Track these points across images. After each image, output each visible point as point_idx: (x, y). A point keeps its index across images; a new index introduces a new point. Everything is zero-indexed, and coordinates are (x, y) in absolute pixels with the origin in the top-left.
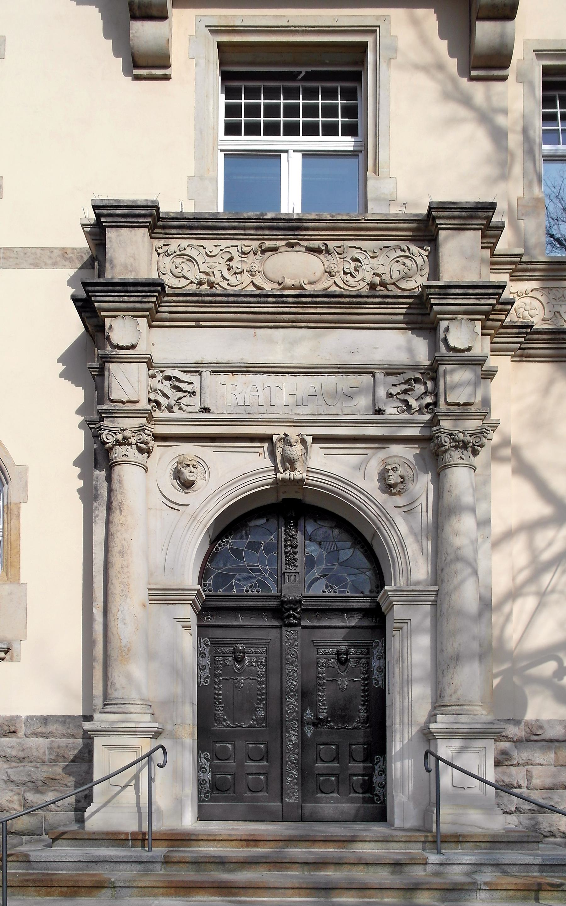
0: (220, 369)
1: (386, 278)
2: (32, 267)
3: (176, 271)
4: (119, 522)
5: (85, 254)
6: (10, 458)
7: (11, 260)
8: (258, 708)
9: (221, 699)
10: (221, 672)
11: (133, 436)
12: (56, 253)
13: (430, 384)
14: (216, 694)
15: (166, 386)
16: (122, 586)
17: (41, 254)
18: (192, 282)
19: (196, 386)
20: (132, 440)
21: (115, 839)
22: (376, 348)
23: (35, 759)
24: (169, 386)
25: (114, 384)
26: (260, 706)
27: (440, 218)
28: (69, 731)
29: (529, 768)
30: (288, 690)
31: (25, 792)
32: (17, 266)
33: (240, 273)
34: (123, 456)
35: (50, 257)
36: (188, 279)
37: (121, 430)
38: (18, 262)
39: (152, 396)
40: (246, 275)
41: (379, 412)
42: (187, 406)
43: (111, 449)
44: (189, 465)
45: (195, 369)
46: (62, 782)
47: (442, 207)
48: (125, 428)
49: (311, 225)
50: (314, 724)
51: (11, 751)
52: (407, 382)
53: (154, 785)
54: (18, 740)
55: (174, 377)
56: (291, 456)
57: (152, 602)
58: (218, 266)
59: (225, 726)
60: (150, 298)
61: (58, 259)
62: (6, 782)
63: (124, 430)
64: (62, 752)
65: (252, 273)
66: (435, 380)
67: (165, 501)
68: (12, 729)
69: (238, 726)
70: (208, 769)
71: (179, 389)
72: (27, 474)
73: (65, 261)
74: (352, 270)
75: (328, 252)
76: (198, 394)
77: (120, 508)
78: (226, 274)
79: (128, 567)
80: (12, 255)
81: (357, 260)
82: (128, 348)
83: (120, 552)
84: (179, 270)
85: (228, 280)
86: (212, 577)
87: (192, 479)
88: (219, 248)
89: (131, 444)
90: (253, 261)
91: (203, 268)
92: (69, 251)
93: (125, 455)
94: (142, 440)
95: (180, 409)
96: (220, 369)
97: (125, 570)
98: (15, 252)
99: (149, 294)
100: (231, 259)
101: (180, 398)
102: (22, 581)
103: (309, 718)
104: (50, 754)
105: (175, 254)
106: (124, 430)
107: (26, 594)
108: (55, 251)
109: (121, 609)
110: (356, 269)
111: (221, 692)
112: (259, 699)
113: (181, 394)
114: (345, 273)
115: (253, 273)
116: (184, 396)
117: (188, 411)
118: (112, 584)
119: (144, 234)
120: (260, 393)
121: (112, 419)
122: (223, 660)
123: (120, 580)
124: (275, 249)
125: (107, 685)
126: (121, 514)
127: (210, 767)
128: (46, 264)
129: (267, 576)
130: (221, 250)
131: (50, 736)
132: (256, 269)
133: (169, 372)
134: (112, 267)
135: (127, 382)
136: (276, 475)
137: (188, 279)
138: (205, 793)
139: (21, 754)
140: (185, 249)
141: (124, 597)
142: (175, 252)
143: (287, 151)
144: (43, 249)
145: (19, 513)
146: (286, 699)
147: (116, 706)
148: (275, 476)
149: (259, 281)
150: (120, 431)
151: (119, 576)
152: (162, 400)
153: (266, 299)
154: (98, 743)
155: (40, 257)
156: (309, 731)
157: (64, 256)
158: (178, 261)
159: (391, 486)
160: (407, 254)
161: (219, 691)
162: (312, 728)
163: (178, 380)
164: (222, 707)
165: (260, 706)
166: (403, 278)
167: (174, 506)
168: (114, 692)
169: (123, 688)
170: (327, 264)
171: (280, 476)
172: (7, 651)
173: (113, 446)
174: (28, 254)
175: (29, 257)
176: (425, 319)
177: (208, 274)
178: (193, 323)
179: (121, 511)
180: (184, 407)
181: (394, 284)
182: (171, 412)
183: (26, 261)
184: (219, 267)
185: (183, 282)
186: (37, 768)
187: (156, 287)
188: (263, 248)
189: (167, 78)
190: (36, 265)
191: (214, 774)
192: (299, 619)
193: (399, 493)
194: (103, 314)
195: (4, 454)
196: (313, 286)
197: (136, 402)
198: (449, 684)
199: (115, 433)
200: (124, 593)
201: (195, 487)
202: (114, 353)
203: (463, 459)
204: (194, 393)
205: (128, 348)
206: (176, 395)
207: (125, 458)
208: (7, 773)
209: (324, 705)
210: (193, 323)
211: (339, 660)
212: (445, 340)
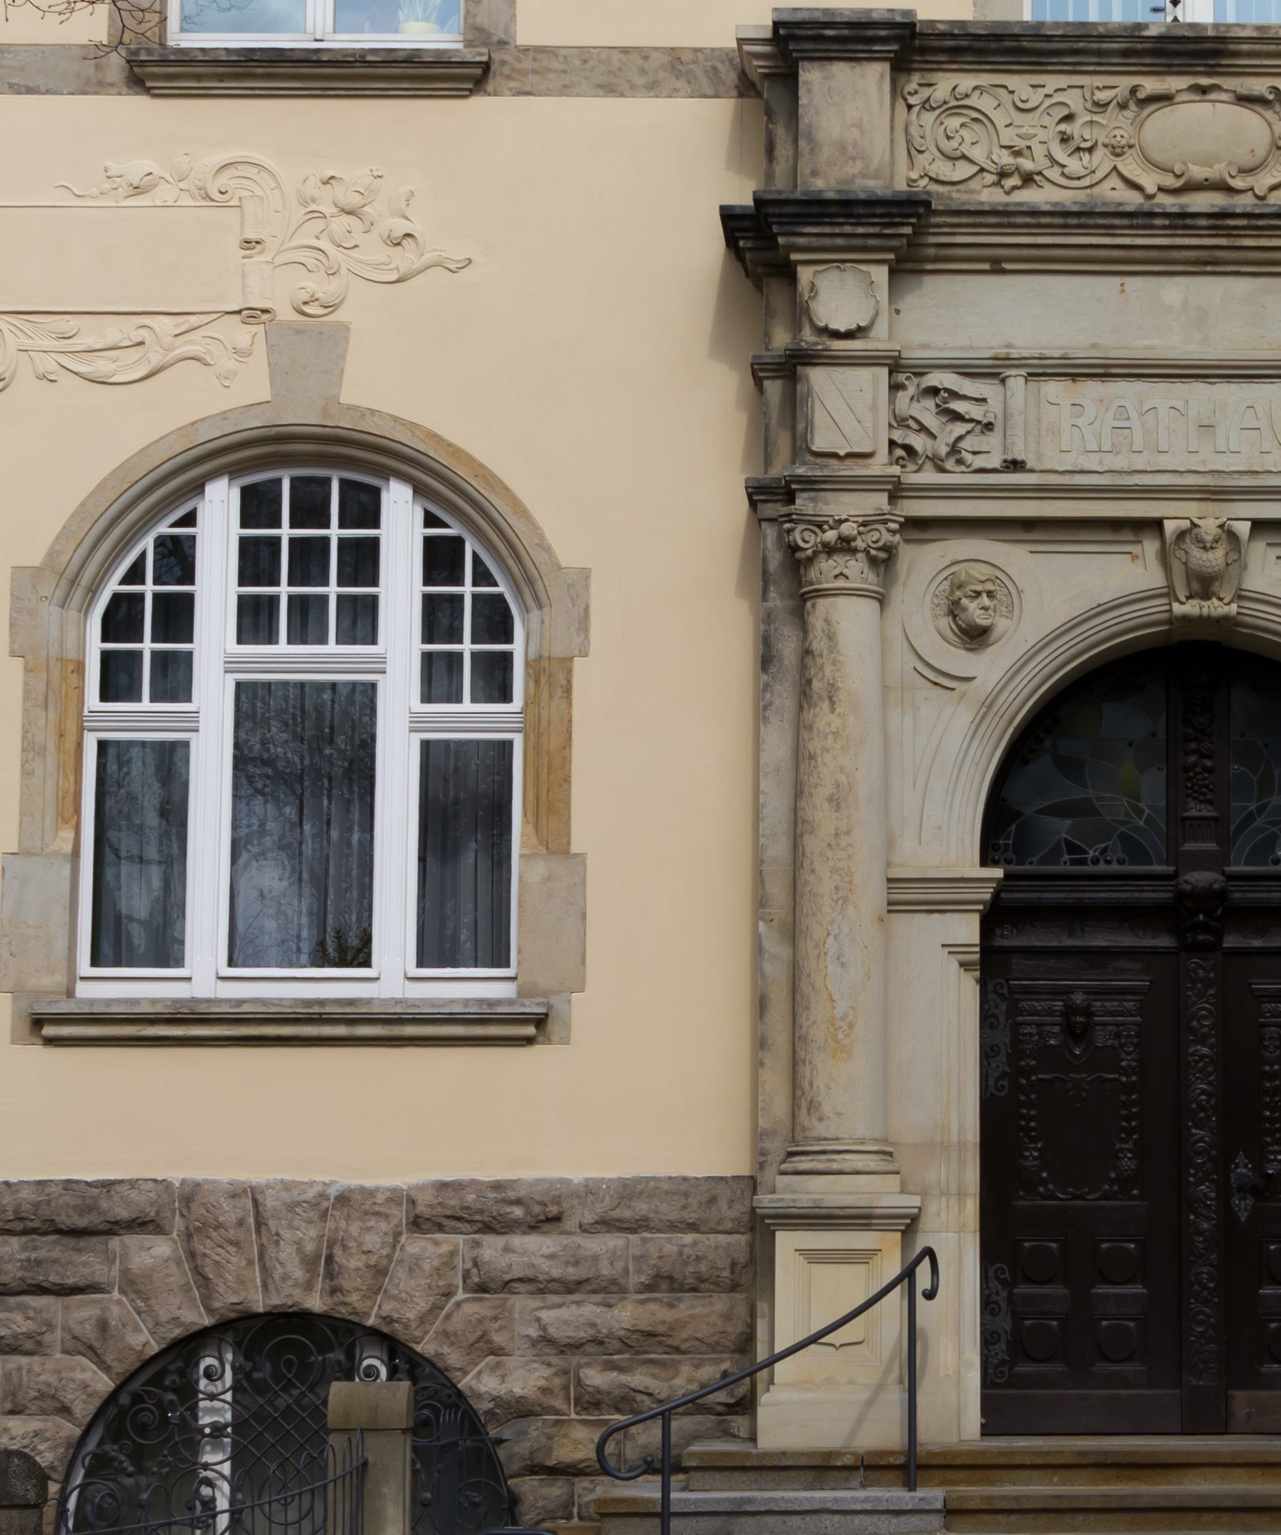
2: (601, 92)
3: (948, 146)
4: (828, 730)
5: (723, 62)
6: (548, 550)
7: (552, 76)
8: (1122, 1150)
9: (1033, 1129)
10: (1033, 1063)
11: (860, 533)
12: (658, 59)
14: (1022, 1117)
15: (926, 412)
16: (836, 877)
17: (621, 62)
18: (982, 170)
20: (859, 544)
23: (604, 1284)
24: (934, 410)
25: (819, 417)
26: (1124, 1146)
30: (1194, 1106)
31: (580, 1366)
32: (565, 90)
34: (836, 577)
35: (643, 71)
36: (974, 163)
37: (836, 521)
38: (567, 82)
39: (898, 436)
40: (1100, 153)
42: (974, 453)
43: (810, 560)
46: (670, 1341)
48: (844, 517)
49: (1245, 47)
51: (550, 1266)
53: (877, 1345)
54: (566, 1240)
55: (946, 390)
56: (1204, 570)
57: (894, 907)
58: (1041, 134)
59: (1044, 1198)
60: (904, 232)
61: (661, 74)
63: (841, 522)
65: (1117, 151)
67: (921, 668)
68: (553, 1210)
69: (1075, 1198)
70: (1004, 1304)
71: (957, 417)
72: (587, 587)
73: (677, 78)
76: (998, 427)
77: (830, 698)
78: (1060, 154)
79: (848, 833)
80: (555, 65)
82: (849, 335)
84: (954, 144)
85: (1064, 166)
86: (1013, 827)
88: (1041, 92)
90: (1118, 125)
91: (1008, 137)
93: (841, 574)
94: (880, 544)
95: (960, 462)
97: (843, 841)
98: (561, 59)
99: (897, 220)
100: (1069, 118)
101: (960, 438)
102: (575, 849)
103: (1244, 1175)
104: (639, 1272)
105: (945, 107)
106: (841, 522)
107: (585, 878)
108: (654, 55)
111: (1033, 1112)
112: (1123, 1130)
113: (960, 428)
115: (1118, 150)
116: (968, 432)
117: (976, 465)
118: (813, 871)
119: (882, 75)
120: (1135, 423)
121: (812, 494)
122: (1040, 1034)
123: (831, 863)
125: (799, 1107)
126: (833, 710)
128: (633, 87)
129: (1141, 823)
130: (1047, 96)
131: (641, 1227)
132: (1124, 142)
133: (935, 379)
134: (812, 150)
135: (847, 408)
136: (1170, 604)
137: (974, 163)
138: (997, 1366)
139: (572, 1273)
140: (967, 96)
141: (840, 902)
142: (945, 102)
144: (625, 51)
145: (569, 682)
146: (1189, 1128)
147: (823, 1157)
148: (1167, 608)
149: (1130, 167)
150: (831, 522)
151: (829, 854)
152: (918, 442)
153: (1148, 221)
154: (787, 1243)
155: (619, 69)
156: (1243, 1206)
157: (673, 67)
161: (1030, 1109)
163: (954, 395)
164: (1036, 1149)
165: (1124, 1146)
167: (944, 681)
168: (814, 1121)
169: (839, 1114)
171: (1178, 609)
173: (815, 553)
174: (591, 63)
175: (592, 69)
177: (1018, 154)
178: (986, 266)
179: (832, 703)
180: (968, 458)
182: (942, 470)
183: (586, 78)
184: (1042, 135)
185: (962, 171)
186: (609, 1306)
187: (912, 208)
188: (1141, 95)
190: (609, 89)
191: (1017, 1318)
192: (1220, 936)
195: (536, 541)
196: (1248, 179)
197: (869, 455)
199: (820, 527)
200: (840, 894)
202: (820, 347)
203: (847, 578)
204: (989, 426)
205: (849, 335)
206: (951, 431)
207: (841, 583)
208: (538, 1320)
210: (986, 266)
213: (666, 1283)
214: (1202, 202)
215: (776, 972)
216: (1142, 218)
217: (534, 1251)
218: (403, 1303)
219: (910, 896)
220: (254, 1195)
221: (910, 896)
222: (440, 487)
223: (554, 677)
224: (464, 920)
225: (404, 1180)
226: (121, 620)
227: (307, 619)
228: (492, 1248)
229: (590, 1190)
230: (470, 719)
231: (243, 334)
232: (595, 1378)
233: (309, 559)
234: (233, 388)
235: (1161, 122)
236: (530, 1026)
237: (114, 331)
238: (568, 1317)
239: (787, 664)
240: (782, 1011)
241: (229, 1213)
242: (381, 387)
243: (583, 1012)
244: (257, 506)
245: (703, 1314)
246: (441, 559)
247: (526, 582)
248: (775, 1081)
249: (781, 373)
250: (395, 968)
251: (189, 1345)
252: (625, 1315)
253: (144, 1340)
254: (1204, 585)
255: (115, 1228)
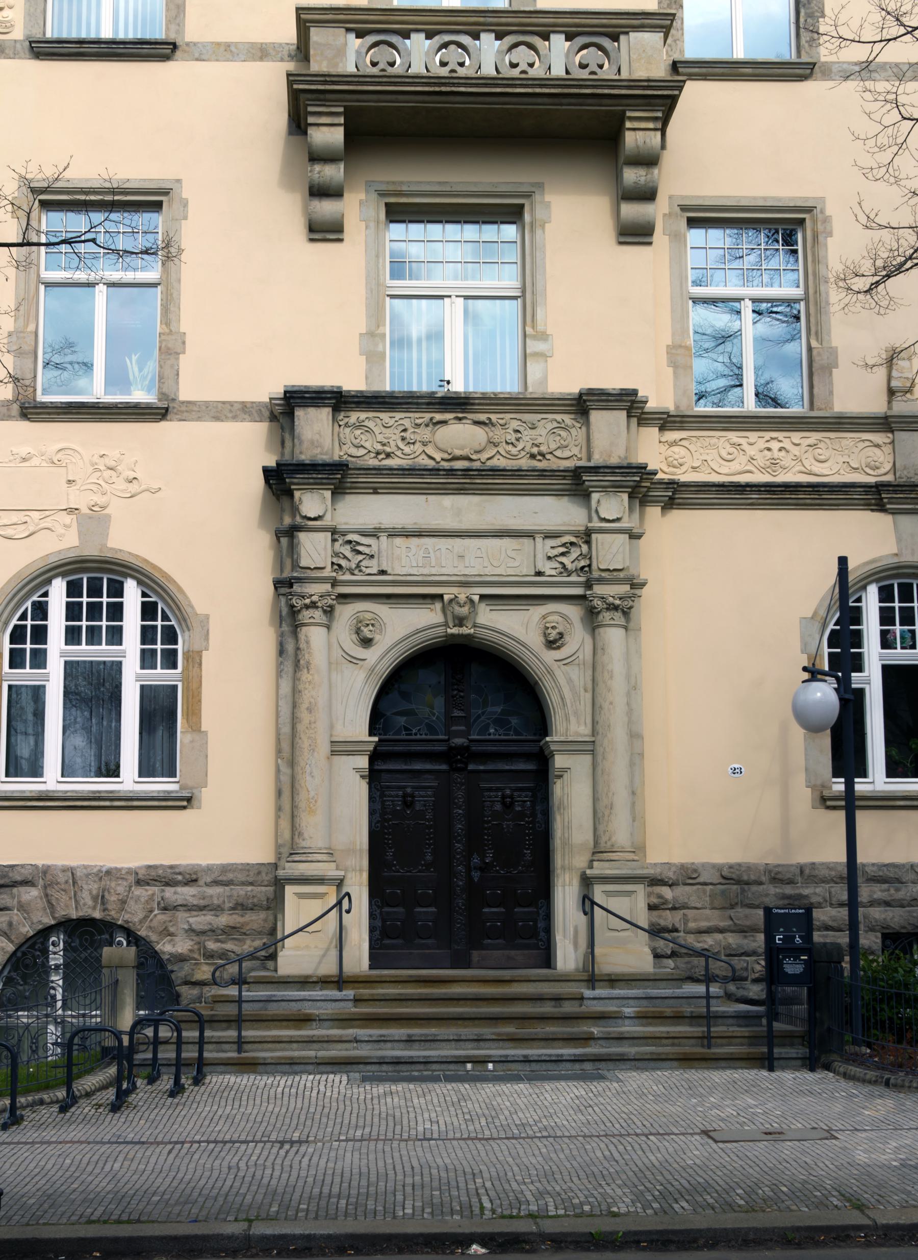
0: (394, 533)
1: (543, 449)
6: (192, 607)
12: (237, 406)
13: (585, 548)
15: (347, 550)
19: (375, 548)
20: (319, 604)
21: (304, 982)
22: (536, 513)
25: (303, 553)
27: (590, 401)
28: (248, 879)
29: (685, 911)
33: (414, 443)
39: (335, 560)
40: (418, 445)
41: (539, 574)
43: (299, 611)
44: (368, 625)
45: (374, 533)
47: (591, 392)
49: (477, 401)
50: (481, 869)
52: (564, 545)
54: (199, 889)
60: (338, 477)
62: (186, 931)
64: (240, 901)
65: (425, 444)
66: (588, 542)
68: (194, 877)
71: (359, 553)
72: (208, 622)
74: (514, 441)
75: (493, 425)
76: (376, 556)
78: (401, 445)
81: (518, 431)
82: (315, 519)
83: (307, 709)
84: (358, 441)
87: (370, 637)
88: (394, 420)
89: (317, 607)
90: (425, 433)
91: (380, 438)
92: (248, 406)
95: (360, 571)
96: (394, 533)
100: (405, 430)
101: (361, 561)
102: (203, 729)
109: (309, 762)
110: (518, 440)
112: (427, 844)
113: (360, 557)
114: (507, 443)
120: (432, 555)
124: (444, 422)
127: (381, 913)
133: (350, 537)
143: (450, 296)
144: (224, 403)
145: (201, 661)
152: (343, 563)
156: (476, 875)
158: (358, 432)
159: (551, 642)
160: (563, 425)
162: (479, 873)
163: (358, 543)
166: (559, 447)
170: (491, 434)
172: (189, 800)
176: (579, 487)
177: (384, 445)
179: (308, 670)
180: (364, 569)
181: (551, 453)
184: (394, 437)
185: (362, 452)
189: (341, 240)
190: (217, 419)
191: (384, 921)
192: (466, 764)
193: (559, 648)
194: (293, 487)
198: (605, 832)
201: (375, 642)
204: (372, 556)
205: (315, 519)
207: (312, 620)
209: (490, 849)
211: (504, 803)
212: (597, 512)
213: (240, 907)
214: (459, 465)
215: (285, 779)
216: (434, 471)
217: (186, 893)
218: (133, 915)
219: (340, 748)
220: (72, 871)
221: (340, 748)
222: (149, 582)
223: (194, 658)
224: (158, 757)
225: (133, 864)
226: (17, 635)
227: (94, 636)
228: (169, 892)
229: (209, 869)
230: (160, 675)
231: (67, 519)
232: (212, 945)
233: (94, 611)
234: (63, 541)
235: (442, 431)
236: (184, 802)
237: (15, 517)
238: (200, 921)
239: (290, 654)
240: (288, 796)
241: (62, 878)
242: (124, 540)
243: (206, 795)
244: (73, 589)
245: (256, 919)
246: (148, 611)
247: (183, 619)
248: (285, 824)
249: (287, 535)
250: (129, 778)
251: (45, 933)
252: (223, 920)
253: (27, 930)
254: (460, 621)
255: (15, 884)
